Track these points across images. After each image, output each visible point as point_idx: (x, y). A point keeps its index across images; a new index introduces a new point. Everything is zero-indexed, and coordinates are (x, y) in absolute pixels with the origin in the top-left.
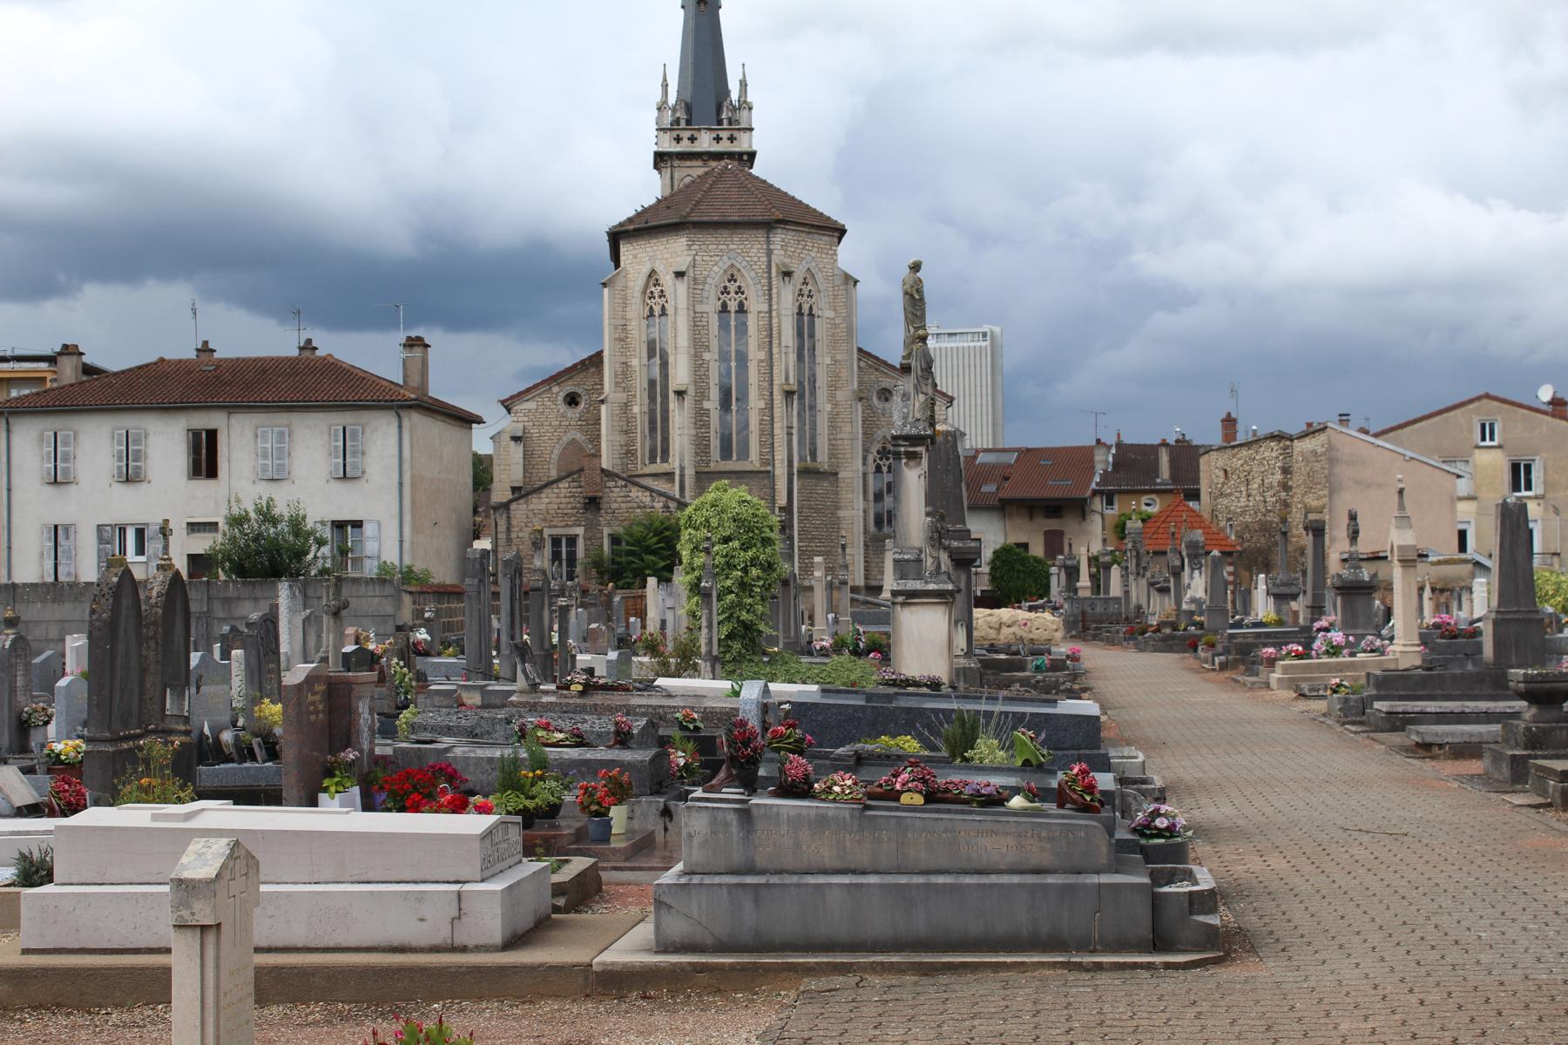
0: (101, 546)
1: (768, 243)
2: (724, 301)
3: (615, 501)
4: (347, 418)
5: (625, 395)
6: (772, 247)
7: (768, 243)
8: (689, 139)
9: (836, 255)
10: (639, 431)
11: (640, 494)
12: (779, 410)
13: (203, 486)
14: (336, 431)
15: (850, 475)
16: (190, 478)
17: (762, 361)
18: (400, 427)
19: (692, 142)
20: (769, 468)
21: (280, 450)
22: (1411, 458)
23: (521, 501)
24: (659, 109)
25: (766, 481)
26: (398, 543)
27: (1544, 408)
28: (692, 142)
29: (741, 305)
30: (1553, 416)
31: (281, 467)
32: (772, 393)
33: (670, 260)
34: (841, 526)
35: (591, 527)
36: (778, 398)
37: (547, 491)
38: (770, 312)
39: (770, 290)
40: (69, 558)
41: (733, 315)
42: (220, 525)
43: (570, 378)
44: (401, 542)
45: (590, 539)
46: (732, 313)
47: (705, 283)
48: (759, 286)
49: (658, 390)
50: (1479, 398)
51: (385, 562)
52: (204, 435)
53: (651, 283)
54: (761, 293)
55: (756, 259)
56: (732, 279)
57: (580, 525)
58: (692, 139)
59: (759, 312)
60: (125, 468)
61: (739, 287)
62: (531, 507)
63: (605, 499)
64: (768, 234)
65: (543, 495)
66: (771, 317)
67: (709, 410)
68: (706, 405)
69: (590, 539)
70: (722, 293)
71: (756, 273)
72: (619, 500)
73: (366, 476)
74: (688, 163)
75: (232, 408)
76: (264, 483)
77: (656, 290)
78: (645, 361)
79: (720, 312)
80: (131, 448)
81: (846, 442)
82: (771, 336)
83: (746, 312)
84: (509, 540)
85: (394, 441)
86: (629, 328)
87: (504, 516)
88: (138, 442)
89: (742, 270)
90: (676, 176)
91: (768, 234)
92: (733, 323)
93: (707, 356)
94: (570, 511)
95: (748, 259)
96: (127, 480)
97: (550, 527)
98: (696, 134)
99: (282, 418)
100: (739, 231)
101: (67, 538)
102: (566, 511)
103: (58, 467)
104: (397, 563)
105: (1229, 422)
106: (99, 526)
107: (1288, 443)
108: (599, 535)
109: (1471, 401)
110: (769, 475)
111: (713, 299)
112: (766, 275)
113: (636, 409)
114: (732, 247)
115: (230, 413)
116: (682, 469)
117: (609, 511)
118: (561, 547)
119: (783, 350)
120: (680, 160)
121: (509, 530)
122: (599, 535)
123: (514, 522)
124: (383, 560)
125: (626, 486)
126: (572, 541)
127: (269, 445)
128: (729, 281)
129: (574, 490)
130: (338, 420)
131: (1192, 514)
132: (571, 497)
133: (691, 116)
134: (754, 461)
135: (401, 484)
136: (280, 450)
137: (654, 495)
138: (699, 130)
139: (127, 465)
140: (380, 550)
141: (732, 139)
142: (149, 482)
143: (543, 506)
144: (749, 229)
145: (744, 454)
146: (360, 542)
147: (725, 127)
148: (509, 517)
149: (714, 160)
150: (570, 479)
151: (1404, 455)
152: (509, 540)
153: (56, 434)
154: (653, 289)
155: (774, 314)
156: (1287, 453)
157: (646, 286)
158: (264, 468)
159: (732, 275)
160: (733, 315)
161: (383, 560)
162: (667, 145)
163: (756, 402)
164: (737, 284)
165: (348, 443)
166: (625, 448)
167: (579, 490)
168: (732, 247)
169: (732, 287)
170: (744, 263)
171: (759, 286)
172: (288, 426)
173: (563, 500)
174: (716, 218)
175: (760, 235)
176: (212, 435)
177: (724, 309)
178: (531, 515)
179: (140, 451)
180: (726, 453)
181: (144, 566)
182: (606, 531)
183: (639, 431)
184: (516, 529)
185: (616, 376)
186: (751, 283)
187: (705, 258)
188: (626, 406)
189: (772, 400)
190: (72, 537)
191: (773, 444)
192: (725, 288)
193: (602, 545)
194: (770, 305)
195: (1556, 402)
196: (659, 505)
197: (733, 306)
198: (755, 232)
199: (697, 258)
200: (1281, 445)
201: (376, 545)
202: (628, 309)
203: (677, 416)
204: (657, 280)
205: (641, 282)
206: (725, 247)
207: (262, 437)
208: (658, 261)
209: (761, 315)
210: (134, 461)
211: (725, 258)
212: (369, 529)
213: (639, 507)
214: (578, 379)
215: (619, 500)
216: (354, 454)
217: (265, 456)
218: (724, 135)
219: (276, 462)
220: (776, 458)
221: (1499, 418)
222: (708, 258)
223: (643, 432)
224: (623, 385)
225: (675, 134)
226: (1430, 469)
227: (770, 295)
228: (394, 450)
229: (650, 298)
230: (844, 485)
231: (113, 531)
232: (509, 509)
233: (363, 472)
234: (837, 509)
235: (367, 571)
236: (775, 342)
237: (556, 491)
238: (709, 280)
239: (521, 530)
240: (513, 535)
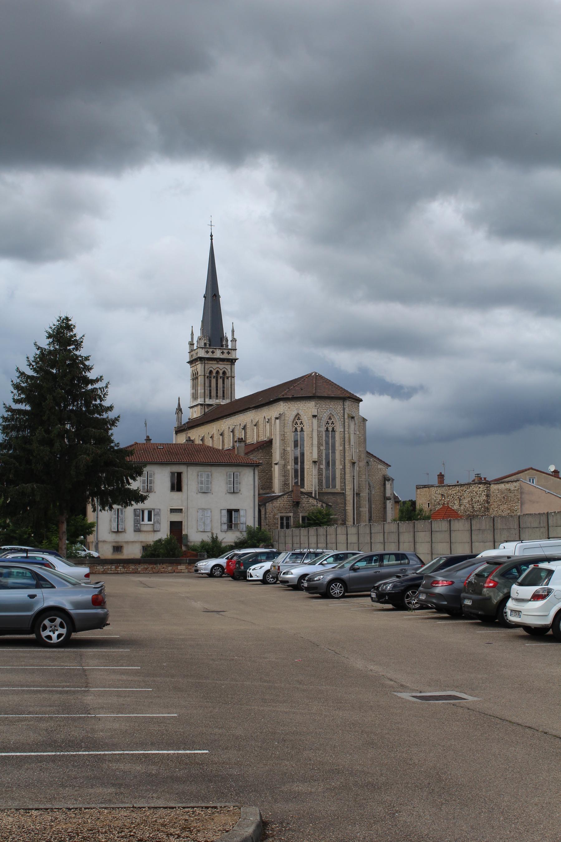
0: (135, 517)
1: (344, 405)
2: (296, 428)
3: (304, 503)
4: (234, 469)
5: (284, 462)
6: (345, 407)
7: (344, 405)
8: (212, 352)
9: (359, 410)
10: (290, 476)
11: (313, 501)
12: (348, 469)
13: (176, 494)
14: (230, 474)
15: (365, 494)
16: (171, 491)
17: (341, 450)
18: (254, 473)
19: (213, 354)
20: (344, 492)
21: (208, 481)
22: (548, 492)
23: (270, 503)
25: (342, 497)
26: (253, 518)
27: (551, 473)
28: (213, 354)
29: (333, 428)
30: (555, 477)
31: (208, 488)
32: (345, 463)
33: (306, 410)
34: (361, 514)
35: (296, 513)
36: (348, 465)
37: (280, 499)
38: (344, 432)
39: (344, 423)
40: (122, 522)
41: (330, 432)
42: (183, 510)
43: (252, 454)
44: (254, 518)
45: (295, 518)
46: (330, 432)
47: (321, 420)
48: (340, 422)
49: (299, 460)
50: (529, 469)
51: (248, 525)
52: (176, 474)
53: (296, 419)
54: (341, 424)
55: (339, 411)
56: (330, 418)
57: (291, 512)
58: (213, 352)
59: (341, 432)
60: (146, 487)
61: (301, 422)
62: (274, 505)
63: (301, 503)
64: (343, 402)
65: (278, 501)
66: (344, 434)
67: (322, 469)
68: (321, 467)
69: (295, 518)
70: (326, 424)
71: (339, 417)
72: (305, 503)
73: (241, 492)
74: (211, 362)
75: (189, 464)
76: (201, 494)
77: (299, 422)
78: (293, 448)
79: (326, 431)
80: (149, 479)
81: (363, 482)
82: (344, 441)
83: (335, 431)
84: (266, 518)
85: (252, 478)
86: (285, 435)
87: (264, 508)
88: (151, 476)
89: (334, 415)
90: (206, 367)
91: (343, 402)
92: (330, 435)
93: (322, 448)
94: (288, 507)
95: (337, 411)
96: (147, 491)
97: (280, 513)
98: (214, 350)
99: (208, 469)
100: (333, 400)
101: (122, 514)
102: (286, 507)
103: (233, 485)
104: (252, 526)
105: (441, 477)
106: (134, 509)
107: (488, 485)
108: (298, 516)
109: (526, 470)
110: (344, 494)
111: (324, 426)
112: (343, 418)
113: (289, 467)
114: (331, 406)
115: (187, 466)
116: (315, 491)
117: (302, 507)
118: (286, 522)
119: (351, 446)
120: (208, 361)
121: (265, 514)
122: (298, 516)
123: (267, 511)
124: (247, 524)
125: (308, 498)
126: (288, 518)
127: (204, 479)
128: (329, 419)
129: (289, 499)
130: (231, 470)
131: (454, 512)
132: (288, 501)
134: (338, 488)
135: (254, 495)
136: (208, 481)
137: (318, 501)
138: (216, 349)
139: (234, 485)
140: (246, 521)
141: (229, 353)
142: (155, 492)
143: (278, 505)
144: (339, 400)
145: (334, 486)
146: (238, 517)
148: (265, 509)
149: (221, 361)
150: (288, 495)
151: (546, 491)
152: (266, 518)
153: (147, 472)
154: (297, 421)
155: (346, 432)
156: (488, 490)
157: (294, 419)
158: (201, 488)
159: (330, 417)
160: (330, 432)
161: (247, 524)
162: (203, 354)
163: (339, 466)
164: (332, 420)
165: (235, 479)
166: (284, 482)
167: (291, 499)
168: (331, 406)
169: (330, 422)
170: (335, 413)
171: (340, 422)
172: (211, 472)
173: (285, 503)
174: (333, 395)
175: (341, 402)
176: (179, 475)
177: (327, 430)
178: (274, 508)
179: (152, 480)
180: (328, 487)
181: (151, 525)
182: (301, 515)
183: (290, 476)
184: (268, 513)
185: (281, 454)
186: (337, 420)
187: (321, 410)
188: (285, 466)
189: (345, 466)
190: (123, 514)
191: (345, 482)
192: (328, 422)
193: (299, 520)
194: (344, 429)
195: (556, 472)
196: (319, 505)
197: (330, 429)
198: (339, 401)
199: (318, 410)
200: (486, 486)
201: (244, 519)
202: (285, 428)
203: (313, 471)
204: (299, 417)
205: (292, 418)
206: (328, 406)
207: (200, 476)
208: (300, 410)
209: (341, 433)
210: (150, 484)
211: (328, 411)
212: (242, 513)
213: (312, 506)
214: (255, 454)
215: (305, 503)
216: (237, 483)
217: (202, 483)
219: (206, 486)
220: (346, 488)
221: (536, 477)
222: (322, 410)
223: (292, 476)
224: (283, 458)
225: (206, 350)
226: (554, 496)
227: (344, 425)
228: (252, 482)
229: (295, 424)
230: (362, 498)
231: (140, 511)
232: (265, 506)
233: (240, 491)
234: (360, 508)
235: (241, 529)
236: (347, 444)
237: (283, 499)
238: (323, 419)
239: (270, 514)
240: (267, 516)
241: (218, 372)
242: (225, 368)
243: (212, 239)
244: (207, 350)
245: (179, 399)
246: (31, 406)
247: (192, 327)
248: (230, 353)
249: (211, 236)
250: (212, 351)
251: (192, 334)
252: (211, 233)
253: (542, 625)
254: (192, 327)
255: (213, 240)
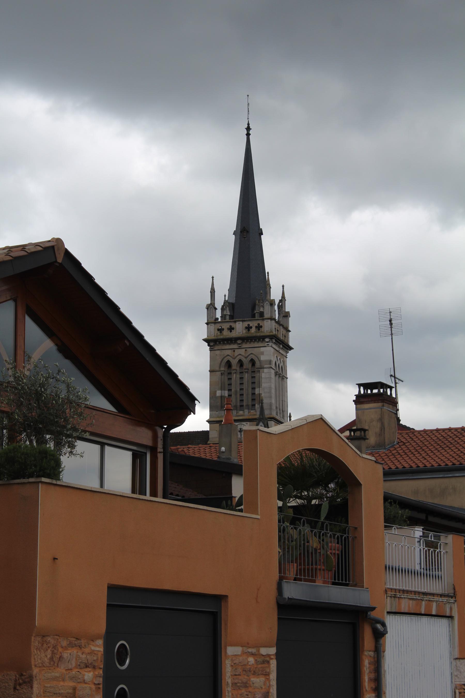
24: (207, 309)
58: (249, 328)
133: (234, 313)
147: (256, 318)
218: (254, 324)
241: (241, 363)
242: (240, 354)
243: (248, 135)
244: (249, 325)
245: (283, 286)
246: (312, 504)
247: (213, 278)
248: (233, 329)
249: (248, 129)
250: (228, 327)
251: (213, 292)
252: (248, 124)
253: (112, 441)
254: (213, 278)
255: (250, 137)
